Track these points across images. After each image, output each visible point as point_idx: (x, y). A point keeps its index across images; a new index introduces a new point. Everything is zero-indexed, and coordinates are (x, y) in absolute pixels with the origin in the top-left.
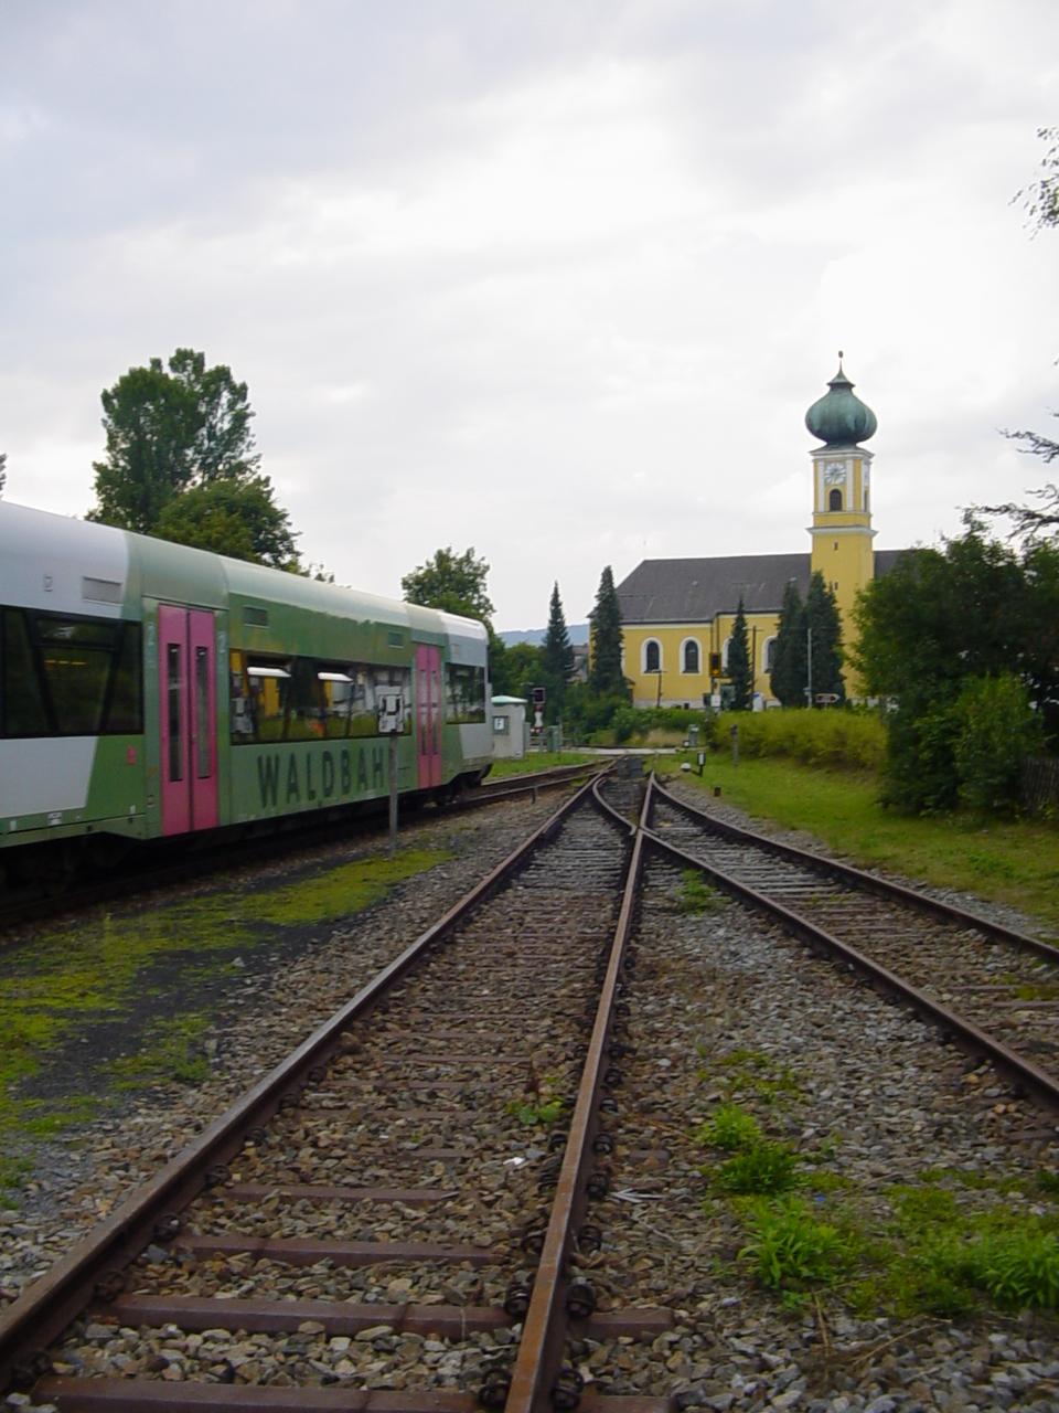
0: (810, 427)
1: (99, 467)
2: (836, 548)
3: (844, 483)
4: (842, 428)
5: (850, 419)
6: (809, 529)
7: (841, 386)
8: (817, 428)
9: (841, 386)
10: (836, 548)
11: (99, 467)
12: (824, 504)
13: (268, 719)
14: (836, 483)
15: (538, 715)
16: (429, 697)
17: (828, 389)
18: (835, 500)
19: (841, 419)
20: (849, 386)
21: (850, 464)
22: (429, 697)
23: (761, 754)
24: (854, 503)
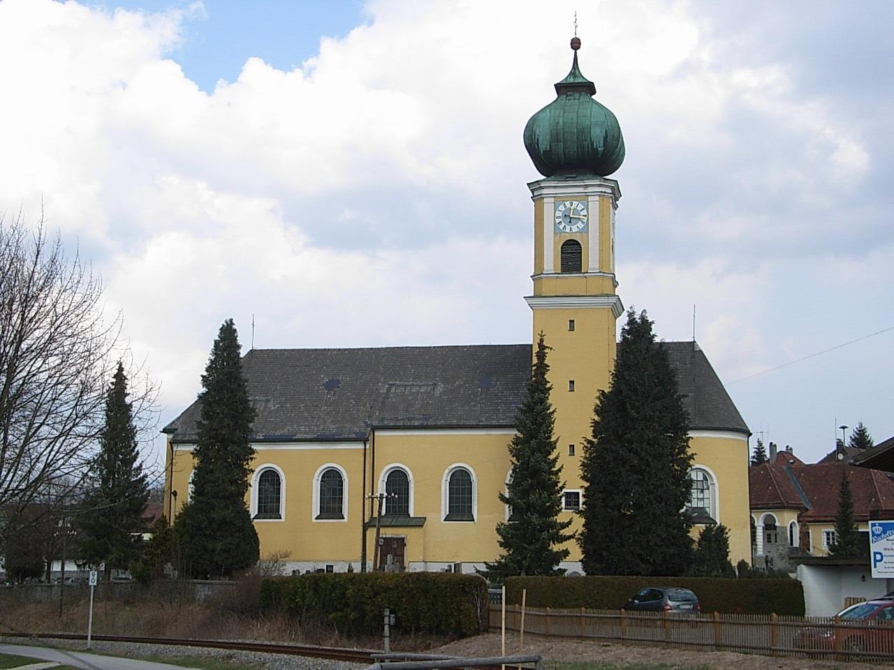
0: (532, 146)
1: (202, 376)
2: (572, 329)
3: (585, 230)
4: (542, 332)
5: (597, 134)
6: (531, 277)
7: (575, 88)
8: (544, 146)
9: (575, 88)
10: (572, 329)
11: (202, 376)
12: (551, 262)
13: (170, 478)
14: (573, 231)
15: (891, 608)
16: (882, 633)
17: (553, 95)
18: (571, 255)
19: (583, 132)
20: (590, 88)
21: (594, 202)
22: (882, 633)
23: (431, 647)
24: (601, 262)
